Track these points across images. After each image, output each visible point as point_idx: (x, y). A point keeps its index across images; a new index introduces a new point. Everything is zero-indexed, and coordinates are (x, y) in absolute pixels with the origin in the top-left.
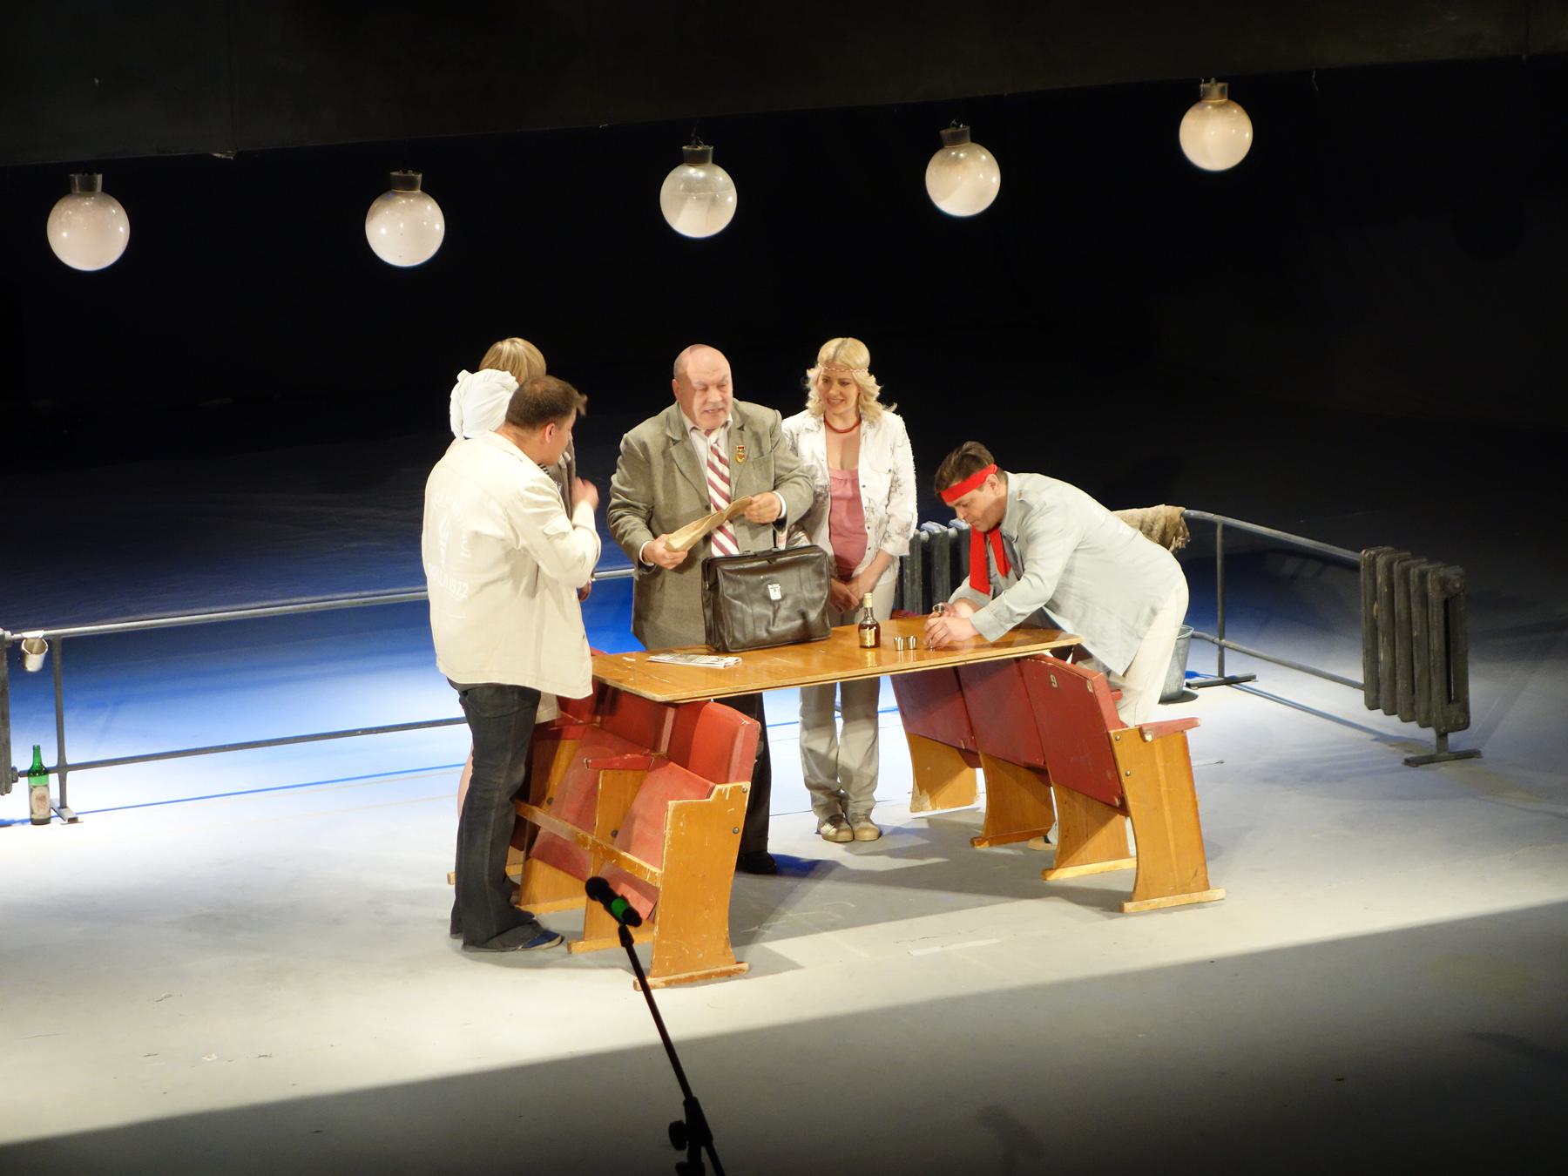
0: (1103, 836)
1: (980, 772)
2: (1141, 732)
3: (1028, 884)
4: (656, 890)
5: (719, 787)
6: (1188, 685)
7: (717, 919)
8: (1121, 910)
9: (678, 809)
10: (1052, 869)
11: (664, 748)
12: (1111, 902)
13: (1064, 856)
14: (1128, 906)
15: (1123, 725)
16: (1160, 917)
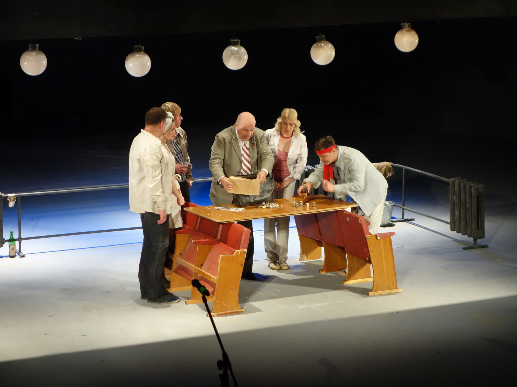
0: (363, 270)
1: (323, 248)
2: (376, 236)
3: (337, 285)
4: (215, 284)
5: (236, 251)
6: (392, 221)
7: (235, 294)
8: (368, 295)
9: (223, 258)
10: (346, 281)
11: (219, 237)
12: (364, 292)
13: (350, 276)
14: (370, 293)
15: (370, 234)
16: (381, 298)
